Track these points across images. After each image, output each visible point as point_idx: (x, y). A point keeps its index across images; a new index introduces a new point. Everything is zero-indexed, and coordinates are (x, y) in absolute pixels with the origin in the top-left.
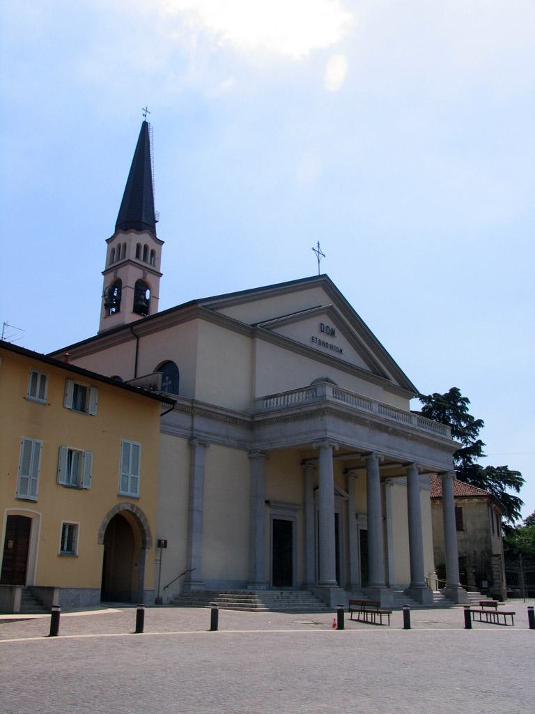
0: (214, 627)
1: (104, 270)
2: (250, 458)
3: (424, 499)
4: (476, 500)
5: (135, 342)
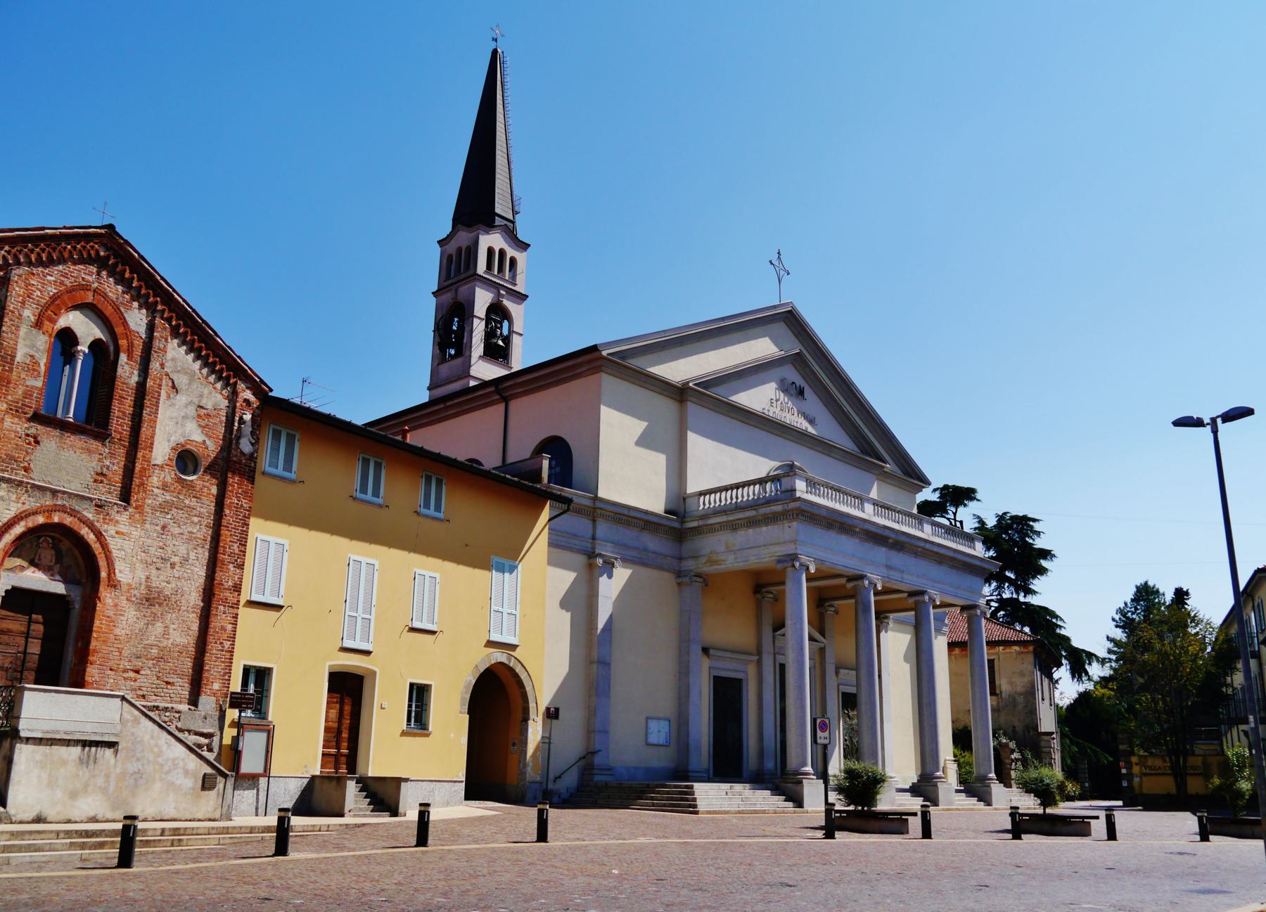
0: (542, 836)
1: (435, 289)
3: (940, 645)
4: (1017, 648)
5: (502, 407)
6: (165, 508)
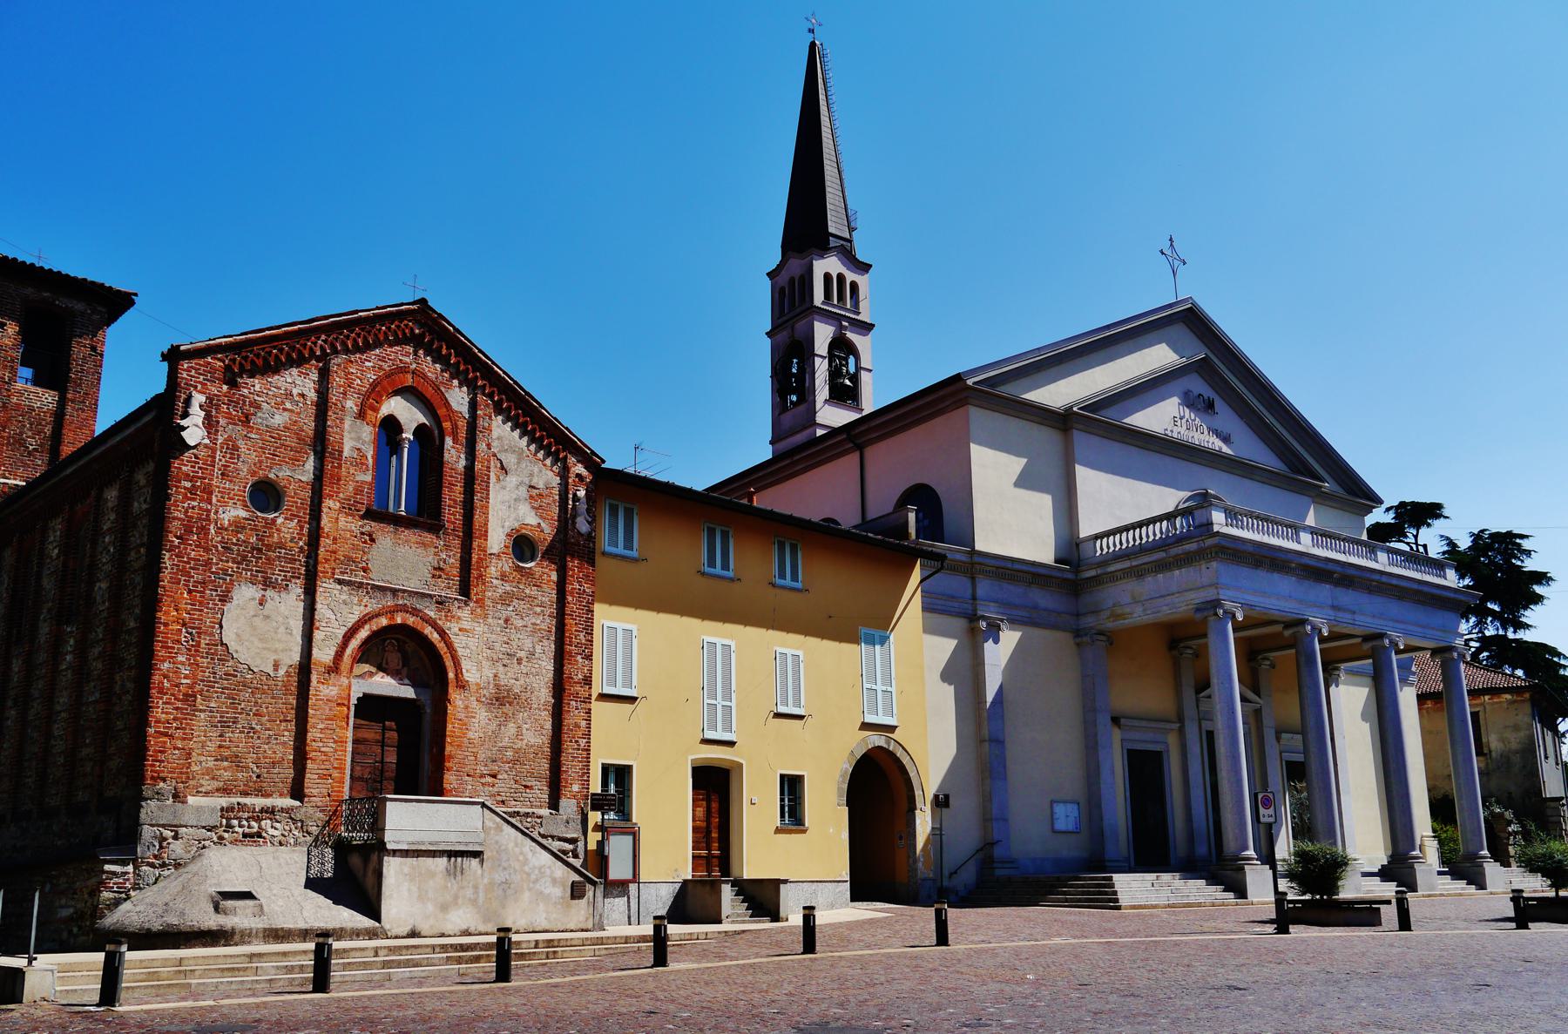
1: (769, 328)
2: (1078, 645)
3: (1407, 699)
5: (856, 456)
6: (506, 599)
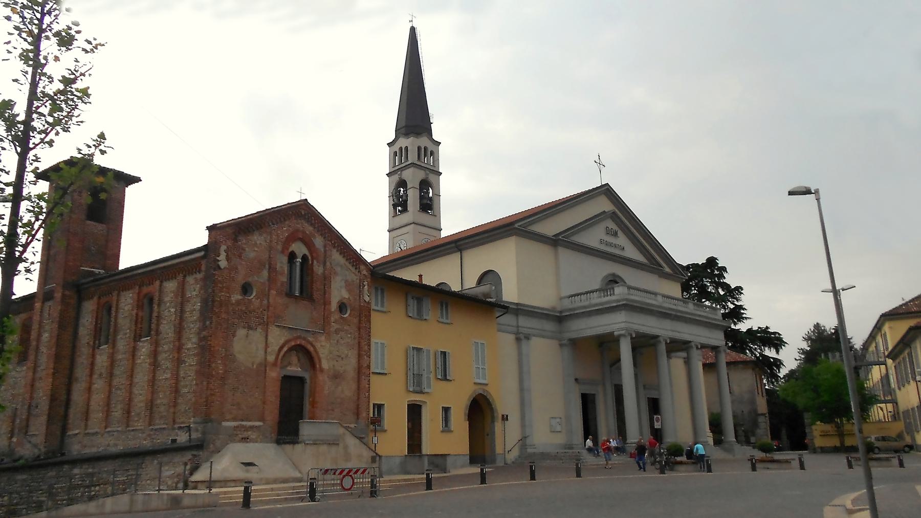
6: (337, 332)
